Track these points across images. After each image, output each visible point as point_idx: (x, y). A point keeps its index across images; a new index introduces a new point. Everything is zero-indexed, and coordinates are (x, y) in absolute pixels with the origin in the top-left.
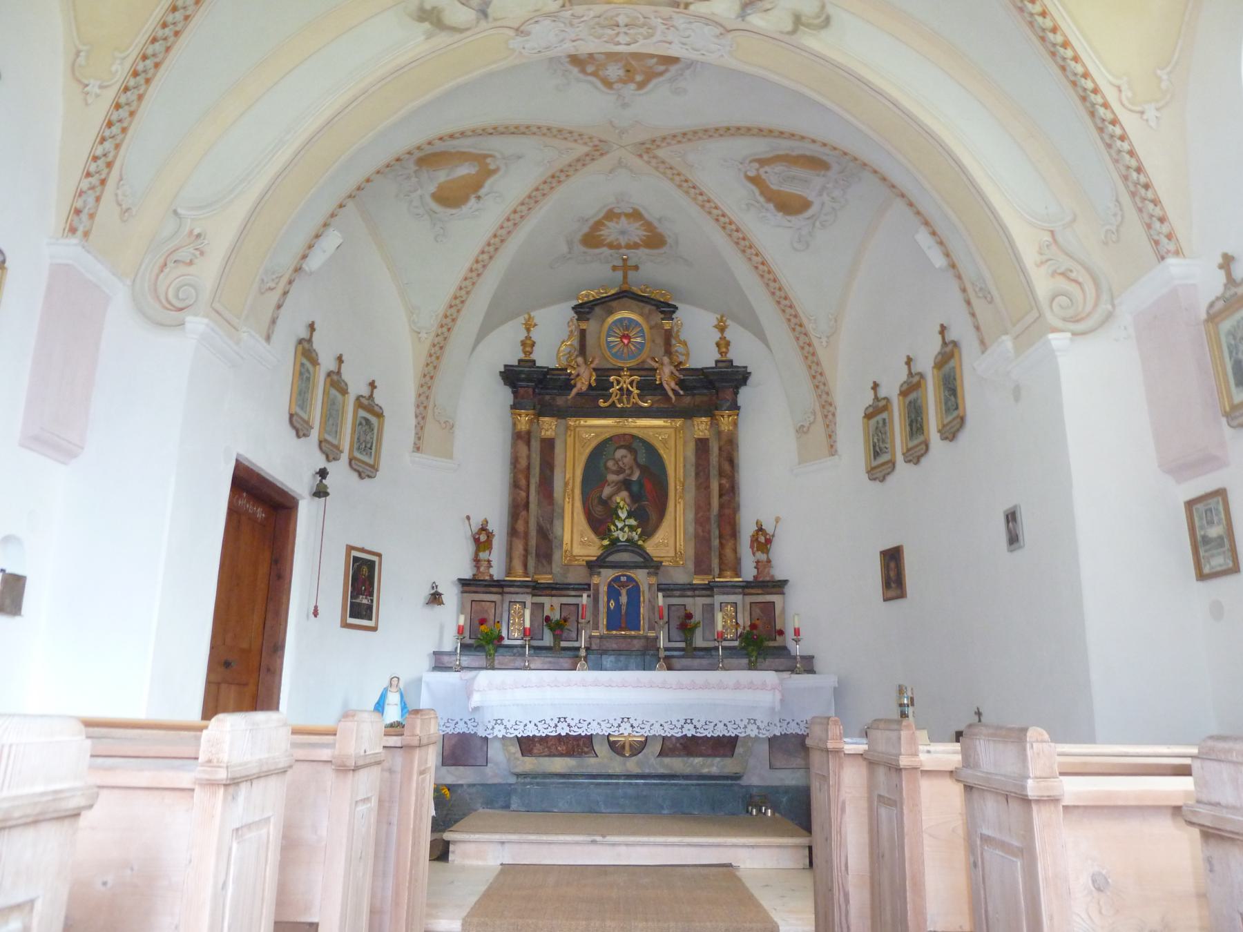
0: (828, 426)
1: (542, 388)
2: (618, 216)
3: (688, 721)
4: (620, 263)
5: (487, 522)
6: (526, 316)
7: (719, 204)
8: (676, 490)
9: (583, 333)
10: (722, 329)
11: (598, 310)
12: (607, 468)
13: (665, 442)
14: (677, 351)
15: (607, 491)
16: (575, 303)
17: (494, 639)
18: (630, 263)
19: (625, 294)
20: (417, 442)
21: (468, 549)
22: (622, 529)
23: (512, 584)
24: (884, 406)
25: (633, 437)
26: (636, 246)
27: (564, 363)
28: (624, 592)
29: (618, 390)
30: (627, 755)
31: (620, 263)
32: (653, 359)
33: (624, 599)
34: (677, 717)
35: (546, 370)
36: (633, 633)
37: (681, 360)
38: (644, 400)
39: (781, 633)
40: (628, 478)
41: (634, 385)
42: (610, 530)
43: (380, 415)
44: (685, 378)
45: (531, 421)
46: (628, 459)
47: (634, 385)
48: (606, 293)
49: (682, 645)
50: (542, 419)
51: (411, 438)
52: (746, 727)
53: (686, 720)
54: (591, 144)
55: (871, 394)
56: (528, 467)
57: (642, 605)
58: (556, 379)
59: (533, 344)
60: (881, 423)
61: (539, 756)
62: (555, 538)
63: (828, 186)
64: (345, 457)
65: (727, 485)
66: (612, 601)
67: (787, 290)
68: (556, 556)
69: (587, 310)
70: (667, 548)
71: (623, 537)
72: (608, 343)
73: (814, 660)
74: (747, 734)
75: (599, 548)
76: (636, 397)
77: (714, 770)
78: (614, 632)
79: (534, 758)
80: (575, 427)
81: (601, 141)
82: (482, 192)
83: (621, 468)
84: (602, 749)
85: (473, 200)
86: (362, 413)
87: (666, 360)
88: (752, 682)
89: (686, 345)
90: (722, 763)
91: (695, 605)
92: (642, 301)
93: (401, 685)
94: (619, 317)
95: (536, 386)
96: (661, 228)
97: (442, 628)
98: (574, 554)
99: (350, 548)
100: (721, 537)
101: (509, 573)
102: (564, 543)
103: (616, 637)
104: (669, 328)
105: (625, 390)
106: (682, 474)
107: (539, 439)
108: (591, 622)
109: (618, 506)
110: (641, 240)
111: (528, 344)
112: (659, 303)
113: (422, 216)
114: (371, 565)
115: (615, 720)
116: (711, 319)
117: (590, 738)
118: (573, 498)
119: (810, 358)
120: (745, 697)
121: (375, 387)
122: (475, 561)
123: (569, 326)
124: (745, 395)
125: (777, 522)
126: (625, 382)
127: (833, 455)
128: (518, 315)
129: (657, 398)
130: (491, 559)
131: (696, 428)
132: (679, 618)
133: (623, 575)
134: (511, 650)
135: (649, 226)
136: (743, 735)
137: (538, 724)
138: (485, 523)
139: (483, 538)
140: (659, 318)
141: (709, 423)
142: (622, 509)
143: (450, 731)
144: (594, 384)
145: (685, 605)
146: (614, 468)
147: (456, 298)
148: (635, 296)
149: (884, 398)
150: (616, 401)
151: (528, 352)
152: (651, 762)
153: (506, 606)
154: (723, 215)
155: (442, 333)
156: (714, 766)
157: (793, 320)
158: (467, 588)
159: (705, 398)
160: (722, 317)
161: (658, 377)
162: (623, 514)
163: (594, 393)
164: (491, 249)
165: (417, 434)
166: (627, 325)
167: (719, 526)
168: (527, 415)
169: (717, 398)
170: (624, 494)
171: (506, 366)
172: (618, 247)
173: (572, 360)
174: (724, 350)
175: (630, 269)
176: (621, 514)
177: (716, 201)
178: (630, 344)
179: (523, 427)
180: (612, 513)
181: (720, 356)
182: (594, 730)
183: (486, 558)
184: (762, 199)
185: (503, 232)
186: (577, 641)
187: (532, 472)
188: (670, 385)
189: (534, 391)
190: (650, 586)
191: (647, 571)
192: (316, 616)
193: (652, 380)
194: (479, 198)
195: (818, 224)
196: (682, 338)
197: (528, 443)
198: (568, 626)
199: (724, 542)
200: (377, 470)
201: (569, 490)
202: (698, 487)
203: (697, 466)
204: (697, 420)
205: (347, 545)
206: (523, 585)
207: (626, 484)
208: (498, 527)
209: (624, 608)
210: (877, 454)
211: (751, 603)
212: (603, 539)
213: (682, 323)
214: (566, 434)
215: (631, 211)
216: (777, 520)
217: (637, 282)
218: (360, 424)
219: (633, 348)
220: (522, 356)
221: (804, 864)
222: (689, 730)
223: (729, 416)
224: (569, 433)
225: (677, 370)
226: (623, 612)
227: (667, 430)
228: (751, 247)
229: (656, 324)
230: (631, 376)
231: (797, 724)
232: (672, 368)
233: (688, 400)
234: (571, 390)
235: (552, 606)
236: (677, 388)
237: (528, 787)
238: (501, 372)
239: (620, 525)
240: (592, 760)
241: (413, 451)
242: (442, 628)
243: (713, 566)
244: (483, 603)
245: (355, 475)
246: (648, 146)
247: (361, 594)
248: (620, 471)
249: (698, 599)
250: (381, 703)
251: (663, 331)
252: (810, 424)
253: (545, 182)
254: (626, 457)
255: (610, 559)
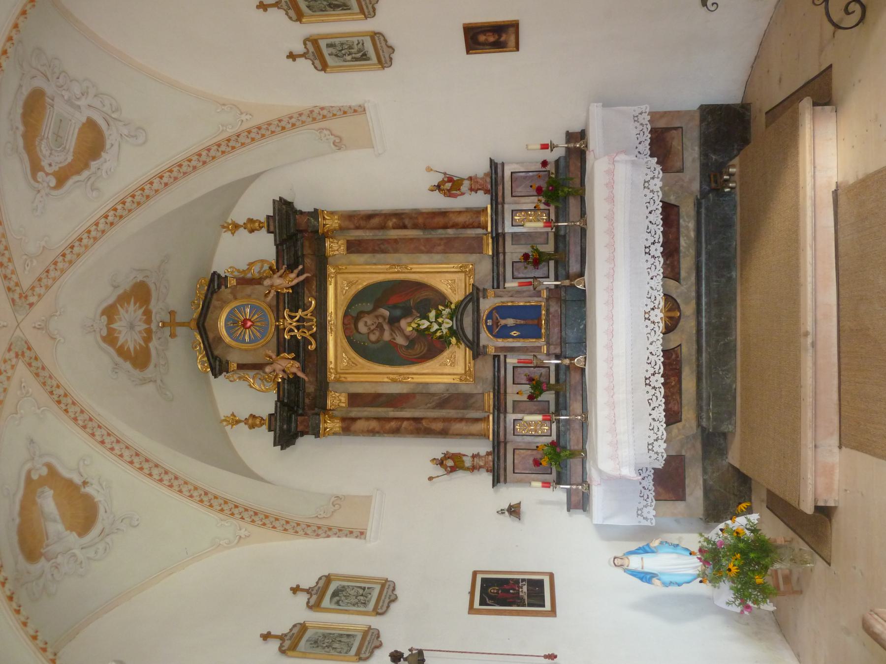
0: (334, 115)
1: (298, 407)
2: (111, 331)
3: (647, 250)
4: (167, 330)
5: (435, 459)
6: (225, 423)
7: (93, 220)
8: (398, 272)
9: (241, 367)
10: (236, 227)
11: (217, 353)
12: (378, 341)
13: (351, 284)
14: (259, 272)
15: (400, 340)
16: (212, 377)
17: (555, 451)
18: (167, 319)
19: (201, 323)
20: (355, 534)
21: (461, 477)
22: (440, 325)
23: (496, 434)
24: (313, 44)
25: (346, 315)
26: (148, 314)
27: (271, 385)
28: (503, 322)
29: (298, 330)
30: (679, 314)
31: (167, 330)
32: (266, 295)
33: (510, 322)
34: (644, 262)
35: (279, 403)
36: (543, 312)
37: (268, 268)
38: (308, 304)
39: (545, 163)
40: (387, 321)
41: (293, 314)
42: (441, 337)
43: (328, 579)
44: (286, 263)
45: (332, 417)
46: (369, 319)
47: (293, 314)
48: (200, 343)
49: (552, 263)
50: (329, 407)
51: (352, 541)
52: (652, 191)
53: (646, 253)
54: (14, 361)
55: (301, 61)
56: (378, 419)
57: (516, 304)
58: (288, 393)
59: (253, 417)
60: (331, 50)
61: (681, 404)
62: (447, 390)
63: (66, 97)
64: (374, 622)
65: (394, 220)
66: (512, 333)
67: (191, 153)
68: (465, 389)
69: (217, 363)
70: (456, 281)
71: (448, 323)
72: (251, 341)
73: (570, 132)
74: (659, 190)
75: (459, 347)
76: (305, 313)
77: (692, 225)
78: (543, 331)
79: (683, 410)
80: (337, 373)
81: (9, 350)
82: (77, 480)
83: (377, 327)
84: (675, 339)
85: (88, 490)
86: (326, 602)
87: (267, 282)
88: (607, 185)
89: (252, 263)
90: (685, 218)
91: (513, 252)
92: (208, 307)
93: (620, 554)
94: (224, 330)
95: (296, 412)
96: (126, 285)
97: (542, 502)
98: (463, 372)
99: (471, 610)
100: (445, 227)
101: (485, 436)
102: (452, 381)
103: (547, 329)
104: (235, 281)
105: (299, 324)
106: (383, 267)
107: (349, 409)
108: (535, 354)
109: (417, 330)
110: (140, 307)
111: (253, 422)
112: (210, 291)
113: (108, 544)
114: (487, 583)
115: (647, 326)
116: (226, 236)
117: (666, 353)
118: (407, 374)
119: (263, 131)
120: (622, 191)
121: (298, 586)
122: (473, 471)
123: (235, 380)
124: (303, 204)
125: (431, 170)
126: (291, 324)
127: (364, 110)
128: (225, 433)
129: (306, 291)
130: (471, 455)
131: (336, 253)
132: (526, 268)
133: (486, 322)
134: (562, 433)
135: (123, 299)
136: (660, 194)
137: (652, 406)
138: (435, 461)
139: (450, 463)
140: (225, 290)
141: (331, 240)
142: (419, 325)
143: (652, 495)
144: (293, 355)
145: (513, 263)
146: (377, 333)
147: (201, 501)
148: (203, 315)
149: (305, 44)
150: (310, 332)
151: (260, 422)
152: (685, 290)
153: (518, 439)
154: (106, 217)
155: (240, 513)
156: (687, 225)
157: (223, 148)
158: (502, 479)
159: (307, 243)
160: (223, 227)
161: (285, 291)
162: (425, 324)
163: (301, 355)
164: (146, 466)
165: (346, 536)
166: (233, 323)
167: (435, 228)
168: (325, 422)
169: (306, 231)
170: (403, 323)
171: (275, 445)
172: (149, 331)
173: (269, 377)
174: (257, 224)
175: (174, 319)
176: (425, 326)
177: (89, 224)
178: (252, 320)
179: (338, 425)
180: (422, 333)
181: (263, 228)
182: (657, 348)
183: (471, 459)
184: (86, 174)
185: (126, 453)
186: (549, 367)
187: (383, 415)
188: (293, 279)
189: (302, 415)
190: (496, 296)
191: (481, 300)
192: (555, 657)
193: (288, 297)
194: (85, 483)
195: (114, 116)
196: (245, 267)
197: (354, 420)
198: (536, 377)
199: (451, 223)
200: (387, 580)
201: (401, 378)
202: (396, 251)
203: (374, 251)
204: (329, 252)
205: (469, 613)
206: (497, 422)
207: (393, 321)
208: (438, 447)
209: (519, 322)
210: (364, 57)
211: (512, 196)
212: (450, 343)
213: (230, 268)
214: (343, 382)
215: (104, 318)
216: (429, 169)
217: (188, 312)
218: (338, 603)
219: (256, 316)
220: (265, 428)
221: (831, 112)
222: (656, 250)
223: (324, 218)
224: (343, 379)
225: (278, 271)
226: (522, 322)
227: (339, 282)
228: (143, 190)
229: (231, 293)
230: (285, 318)
231: (640, 143)
232: (275, 276)
233: (308, 261)
234: (299, 377)
235: (518, 393)
236: (296, 271)
237: (711, 414)
238: (282, 449)
239: (435, 327)
240: (684, 349)
241: (365, 538)
242: (542, 502)
243: (474, 236)
244: (516, 461)
245: (393, 606)
246: (16, 297)
247: (519, 594)
248: (380, 327)
249: (507, 250)
250: (642, 575)
251: (238, 286)
252: (332, 135)
253: (66, 411)
254: (366, 322)
255: (470, 336)
